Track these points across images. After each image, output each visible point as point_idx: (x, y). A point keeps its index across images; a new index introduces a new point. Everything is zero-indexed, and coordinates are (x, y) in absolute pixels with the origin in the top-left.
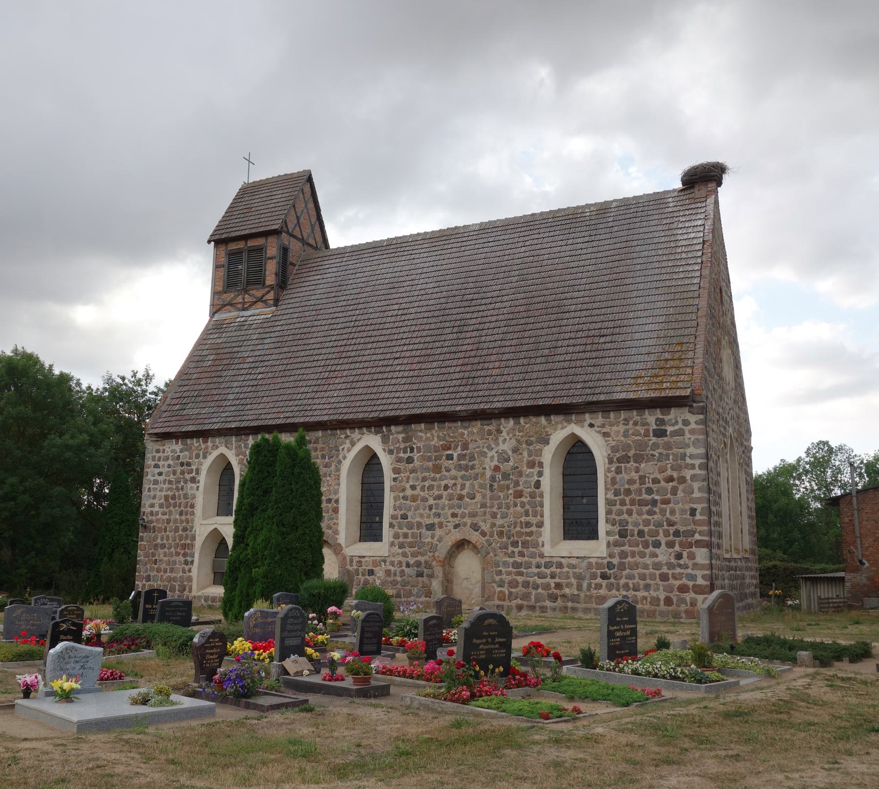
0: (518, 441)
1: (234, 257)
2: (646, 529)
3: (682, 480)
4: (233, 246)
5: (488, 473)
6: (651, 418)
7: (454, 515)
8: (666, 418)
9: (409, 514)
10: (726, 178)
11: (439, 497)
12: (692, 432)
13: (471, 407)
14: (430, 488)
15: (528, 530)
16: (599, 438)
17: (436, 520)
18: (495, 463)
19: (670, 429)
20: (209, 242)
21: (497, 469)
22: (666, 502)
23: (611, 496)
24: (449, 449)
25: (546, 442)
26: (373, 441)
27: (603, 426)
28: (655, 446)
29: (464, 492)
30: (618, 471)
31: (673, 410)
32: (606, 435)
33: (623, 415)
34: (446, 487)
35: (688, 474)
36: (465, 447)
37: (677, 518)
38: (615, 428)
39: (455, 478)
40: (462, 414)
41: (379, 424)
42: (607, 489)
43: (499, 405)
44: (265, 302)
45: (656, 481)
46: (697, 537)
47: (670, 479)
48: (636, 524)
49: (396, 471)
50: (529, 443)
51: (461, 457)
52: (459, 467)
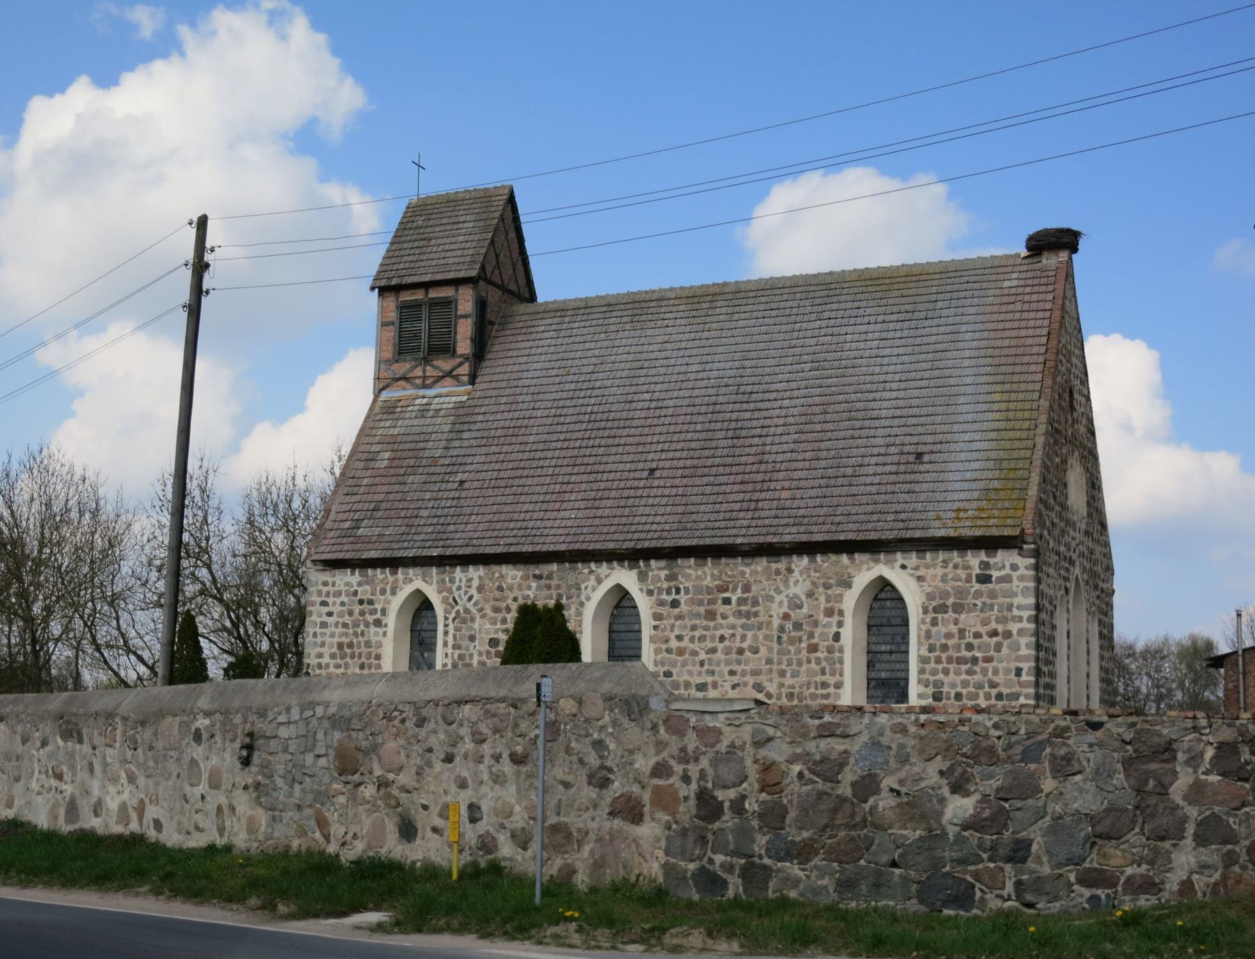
0: (814, 583)
1: (408, 312)
2: (964, 691)
3: (1008, 634)
4: (407, 297)
5: (776, 622)
6: (974, 560)
7: (732, 673)
8: (992, 561)
9: (674, 671)
10: (1082, 244)
11: (713, 651)
12: (1021, 578)
13: (755, 540)
14: (702, 639)
15: (824, 692)
16: (913, 583)
17: (709, 679)
18: (785, 609)
19: (995, 574)
20: (373, 289)
21: (786, 617)
22: (989, 660)
23: (924, 652)
24: (726, 590)
25: (848, 585)
26: (626, 577)
27: (917, 568)
28: (978, 594)
29: (745, 645)
30: (934, 622)
31: (1000, 552)
32: (920, 579)
33: (942, 555)
34: (722, 639)
35: (1014, 627)
36: (747, 588)
37: (1000, 679)
38: (931, 571)
39: (734, 627)
40: (744, 548)
41: (634, 557)
42: (920, 643)
43: (788, 538)
44: (456, 377)
45: (977, 635)
46: (1022, 700)
47: (994, 633)
48: (953, 685)
49: (657, 617)
50: (827, 586)
51: (741, 601)
52: (739, 614)
